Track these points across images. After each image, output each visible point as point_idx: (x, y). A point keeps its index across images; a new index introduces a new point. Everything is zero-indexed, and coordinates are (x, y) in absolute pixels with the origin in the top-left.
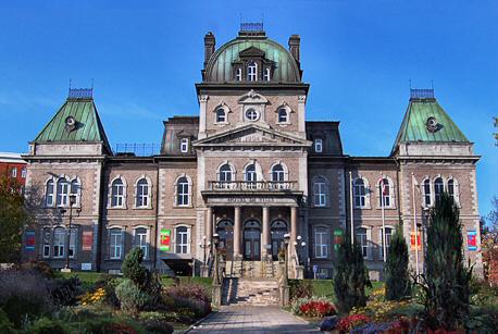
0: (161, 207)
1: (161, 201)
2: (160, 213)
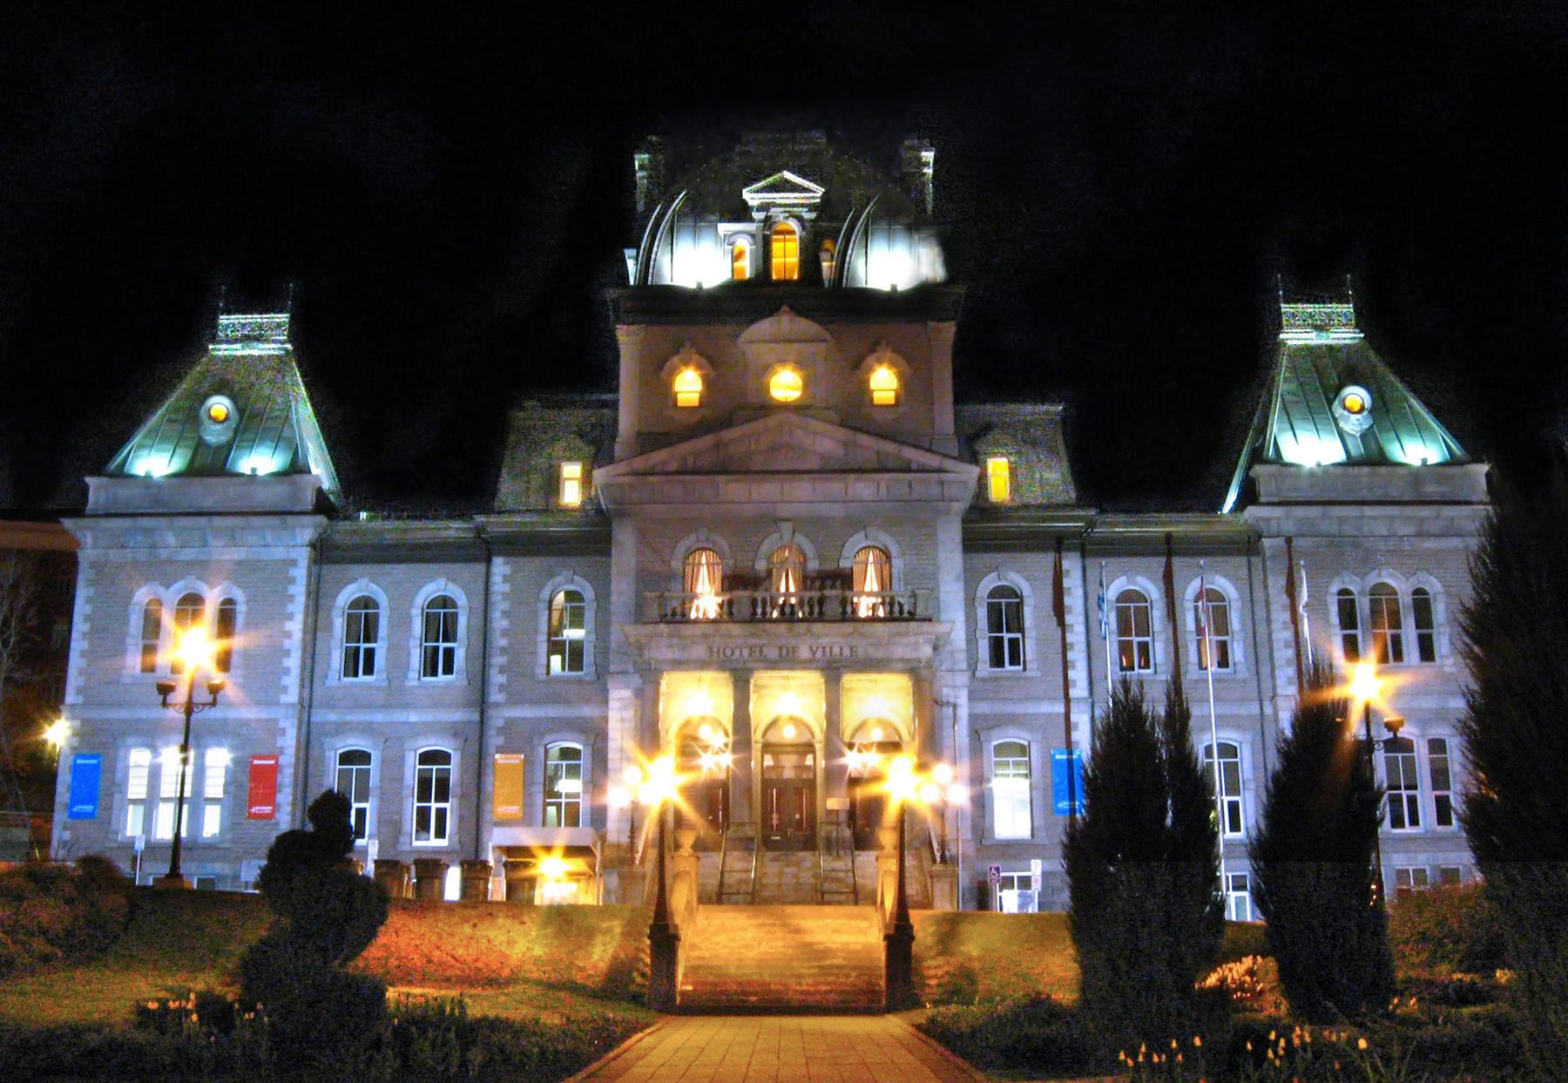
0: (497, 679)
1: (498, 660)
2: (495, 696)
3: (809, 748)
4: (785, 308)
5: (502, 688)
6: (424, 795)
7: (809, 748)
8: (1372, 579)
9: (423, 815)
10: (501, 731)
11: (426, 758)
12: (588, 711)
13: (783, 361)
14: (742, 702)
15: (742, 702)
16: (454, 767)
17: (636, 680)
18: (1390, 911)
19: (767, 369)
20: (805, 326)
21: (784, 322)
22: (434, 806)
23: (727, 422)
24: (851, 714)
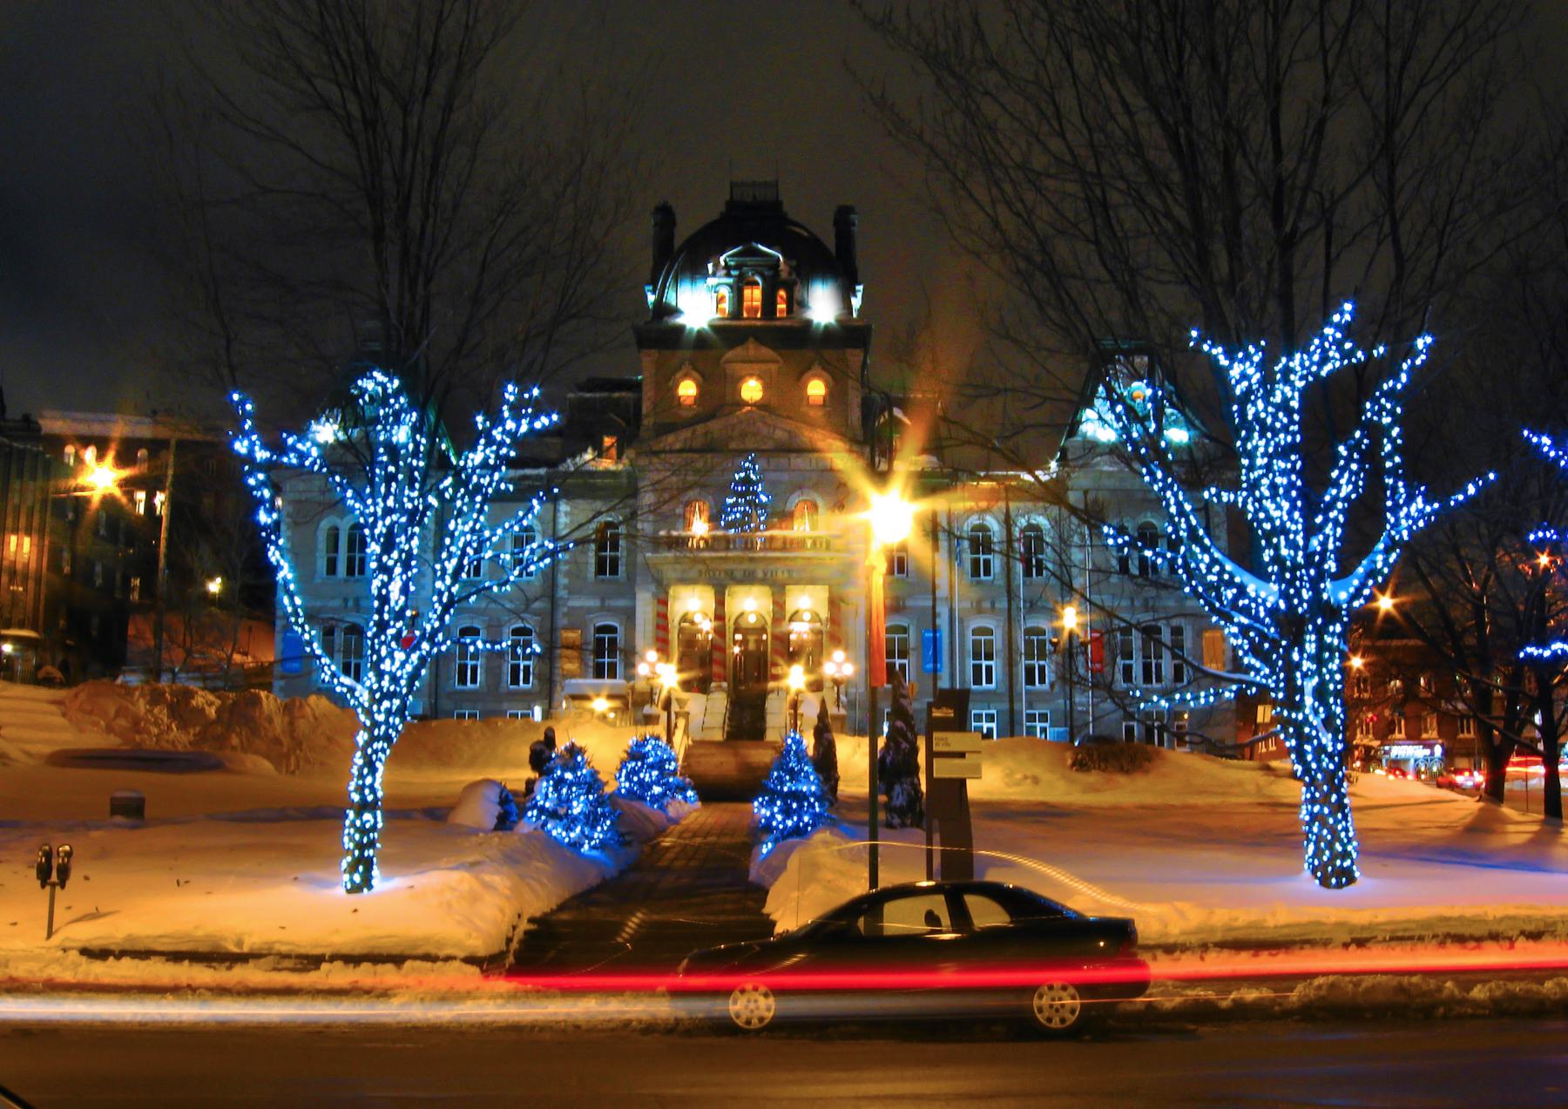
0: (562, 581)
2: (562, 593)
3: (763, 630)
4: (751, 340)
5: (565, 587)
6: (977, 656)
7: (763, 630)
8: (1142, 520)
9: (977, 668)
10: (565, 615)
11: (601, 630)
12: (621, 603)
13: (751, 375)
14: (720, 603)
15: (720, 603)
16: (912, 637)
17: (653, 587)
18: (119, 681)
19: (738, 381)
20: (766, 352)
21: (752, 349)
22: (984, 663)
23: (711, 416)
24: (790, 608)
